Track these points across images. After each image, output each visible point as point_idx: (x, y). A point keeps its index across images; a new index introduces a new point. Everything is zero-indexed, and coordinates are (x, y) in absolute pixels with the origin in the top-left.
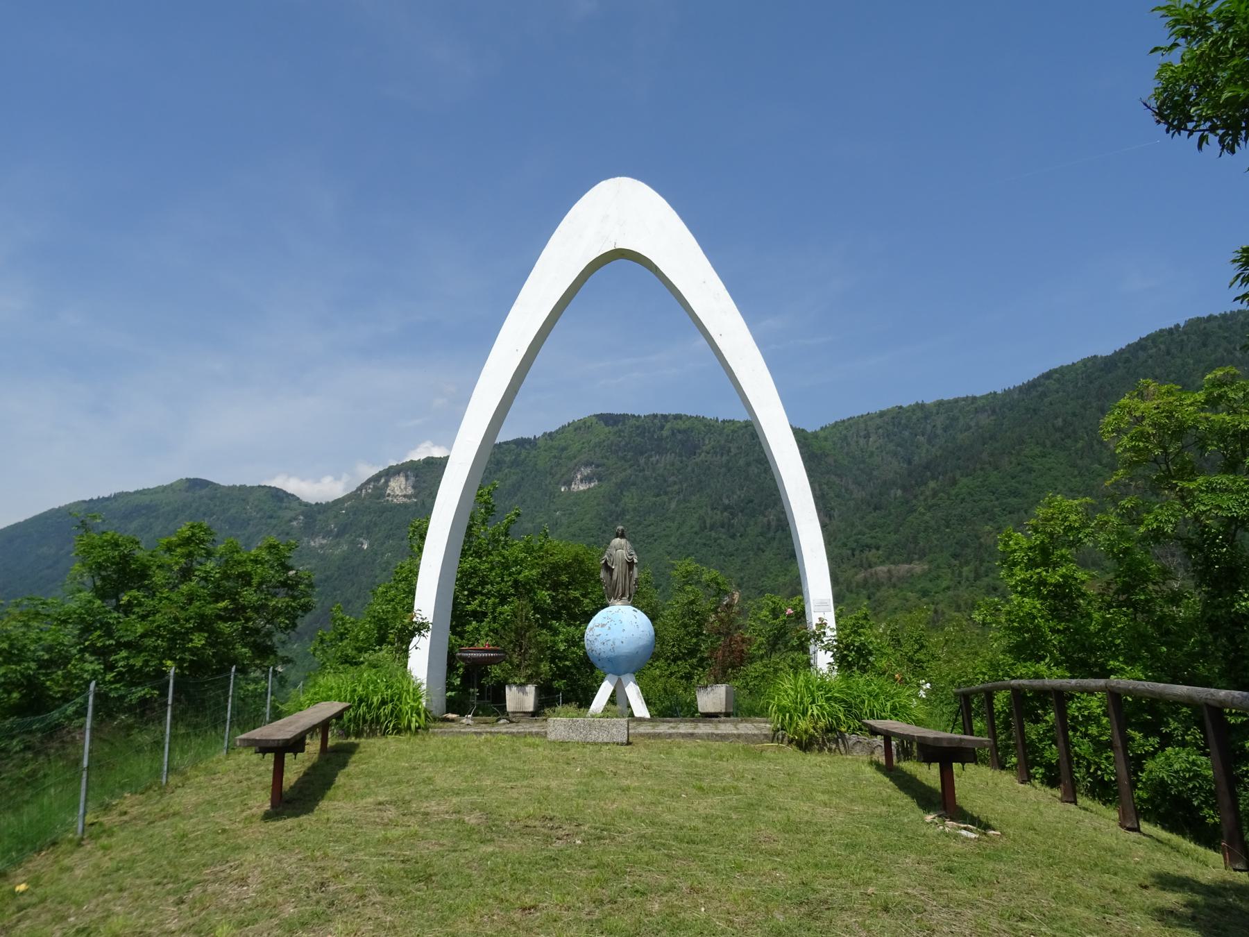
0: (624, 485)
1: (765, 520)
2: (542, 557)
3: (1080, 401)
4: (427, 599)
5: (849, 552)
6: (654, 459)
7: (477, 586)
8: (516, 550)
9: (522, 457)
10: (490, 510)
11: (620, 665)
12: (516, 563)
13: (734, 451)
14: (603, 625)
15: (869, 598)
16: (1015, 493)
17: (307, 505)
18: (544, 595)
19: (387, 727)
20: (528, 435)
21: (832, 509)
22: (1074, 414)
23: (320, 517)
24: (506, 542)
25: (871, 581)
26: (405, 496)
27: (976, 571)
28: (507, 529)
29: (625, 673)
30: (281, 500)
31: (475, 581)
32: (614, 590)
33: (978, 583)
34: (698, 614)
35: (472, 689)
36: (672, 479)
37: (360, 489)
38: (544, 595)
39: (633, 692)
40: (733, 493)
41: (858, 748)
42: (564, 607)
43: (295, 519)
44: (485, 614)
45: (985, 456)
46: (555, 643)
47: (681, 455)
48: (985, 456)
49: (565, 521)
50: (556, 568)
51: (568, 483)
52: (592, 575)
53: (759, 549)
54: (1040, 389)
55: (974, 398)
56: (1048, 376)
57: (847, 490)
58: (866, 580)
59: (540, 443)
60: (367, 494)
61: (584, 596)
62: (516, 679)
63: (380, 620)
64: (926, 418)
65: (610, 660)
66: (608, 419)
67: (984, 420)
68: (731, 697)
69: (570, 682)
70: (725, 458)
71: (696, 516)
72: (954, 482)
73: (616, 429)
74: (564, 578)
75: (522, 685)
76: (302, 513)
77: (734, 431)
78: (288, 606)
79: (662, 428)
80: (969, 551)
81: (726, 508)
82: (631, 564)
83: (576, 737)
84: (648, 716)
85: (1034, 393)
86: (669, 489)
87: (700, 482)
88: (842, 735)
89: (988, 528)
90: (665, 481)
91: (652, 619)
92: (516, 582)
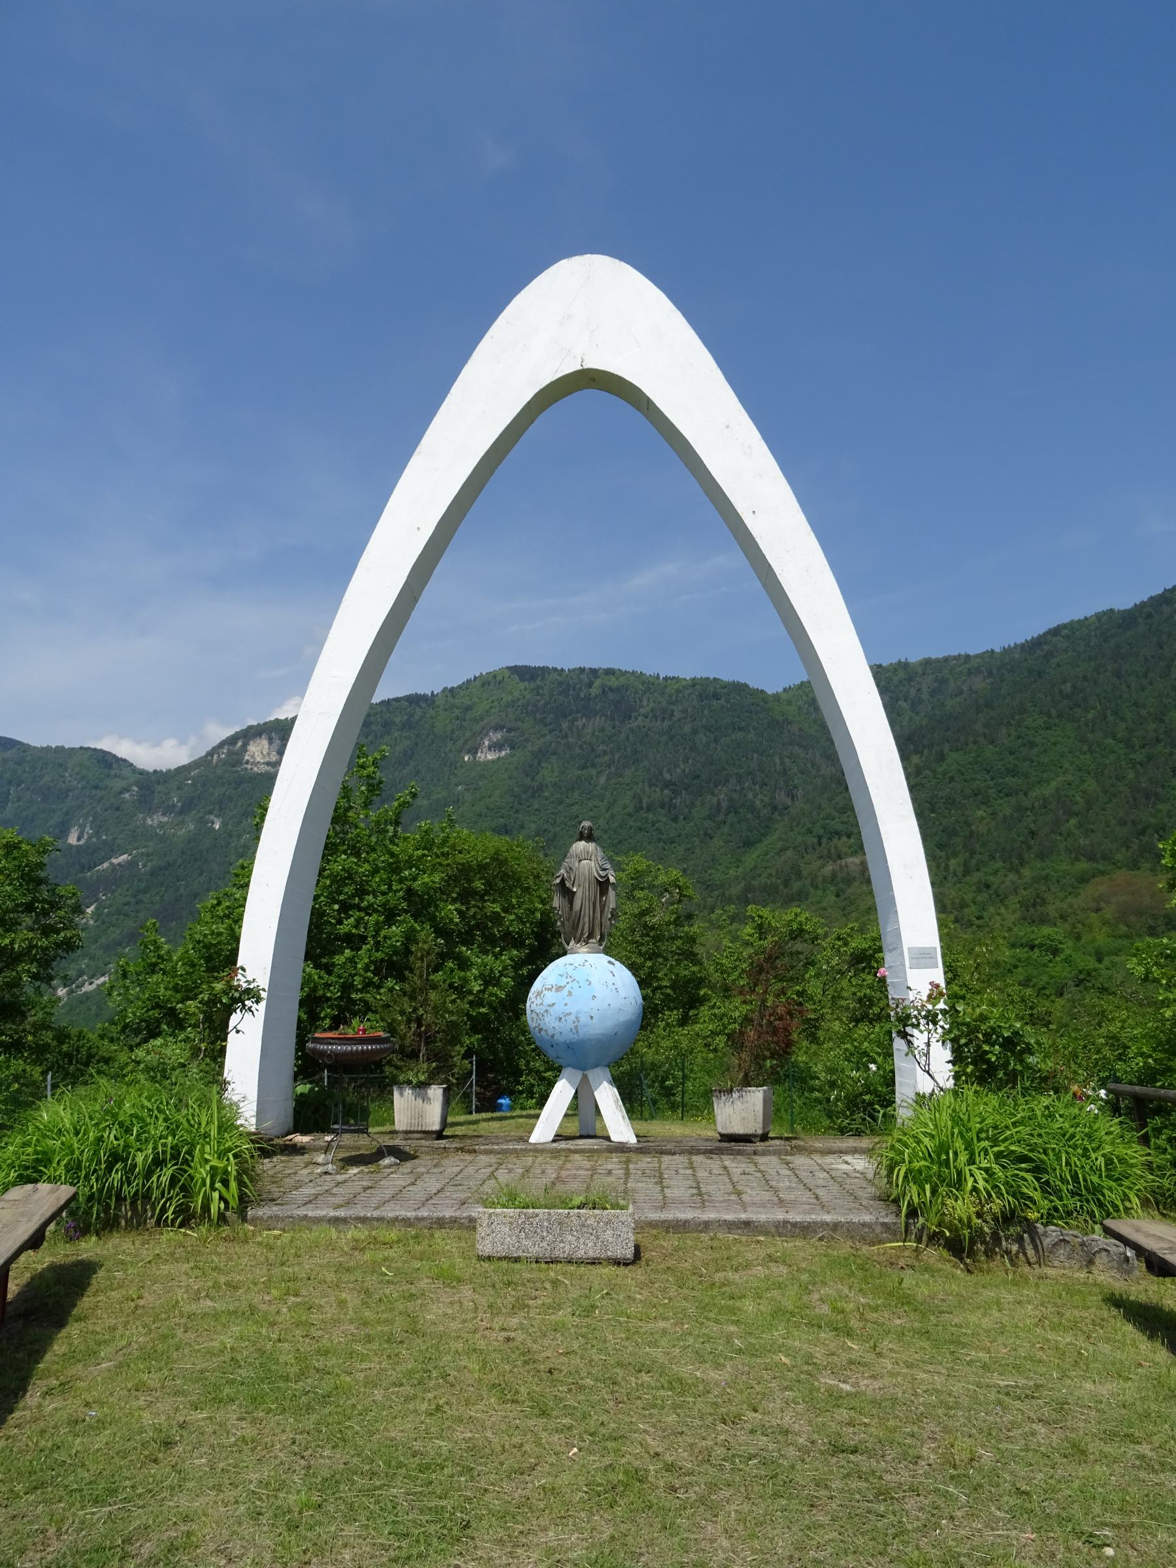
0: (541, 755)
1: (715, 800)
2: (446, 855)
3: (1093, 664)
4: (258, 951)
5: (815, 840)
6: (579, 723)
7: (353, 896)
8: (407, 847)
9: (417, 717)
10: (374, 787)
11: (581, 1055)
12: (410, 864)
13: (677, 715)
14: (559, 989)
15: (838, 896)
16: (1014, 772)
17: (142, 773)
18: (450, 911)
19: (164, 1210)
20: (424, 689)
21: (795, 787)
22: (1085, 678)
23: (159, 788)
24: (395, 835)
25: (840, 875)
26: (268, 764)
27: (965, 865)
28: (398, 815)
29: (596, 1066)
30: (109, 766)
31: (349, 889)
32: (575, 927)
33: (968, 878)
34: (652, 928)
35: (331, 1092)
36: (602, 747)
37: (210, 754)
38: (450, 911)
39: (607, 1097)
40: (676, 766)
41: (1062, 1252)
42: (478, 926)
43: (127, 790)
44: (363, 939)
45: (978, 727)
46: (465, 981)
47: (612, 719)
48: (978, 727)
49: (468, 797)
50: (466, 871)
51: (473, 751)
52: (519, 880)
53: (706, 834)
54: (1046, 647)
55: (968, 657)
56: (1055, 632)
57: (813, 764)
58: (834, 875)
59: (440, 701)
60: (220, 760)
61: (506, 910)
62: (411, 1076)
63: (208, 947)
64: (910, 680)
65: (570, 1046)
66: (523, 673)
67: (980, 684)
68: (772, 1113)
69: (501, 1067)
70: (666, 724)
71: (630, 793)
72: (941, 758)
73: (533, 685)
74: (479, 885)
75: (422, 1086)
76: (137, 783)
77: (678, 691)
78: (31, 947)
79: (590, 685)
80: (957, 840)
81: (667, 785)
82: (603, 886)
83: (534, 1249)
84: (633, 1140)
85: (1039, 653)
86: (598, 760)
87: (635, 752)
88: (1030, 1227)
89: (980, 813)
90: (593, 750)
91: (642, 983)
92: (409, 891)
